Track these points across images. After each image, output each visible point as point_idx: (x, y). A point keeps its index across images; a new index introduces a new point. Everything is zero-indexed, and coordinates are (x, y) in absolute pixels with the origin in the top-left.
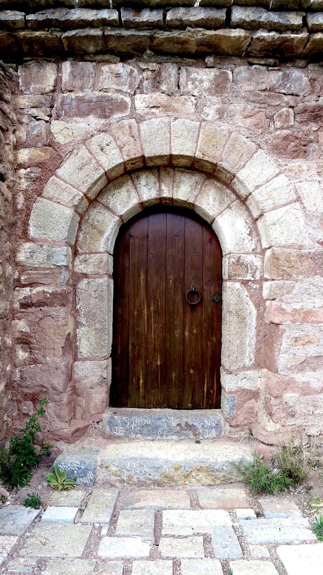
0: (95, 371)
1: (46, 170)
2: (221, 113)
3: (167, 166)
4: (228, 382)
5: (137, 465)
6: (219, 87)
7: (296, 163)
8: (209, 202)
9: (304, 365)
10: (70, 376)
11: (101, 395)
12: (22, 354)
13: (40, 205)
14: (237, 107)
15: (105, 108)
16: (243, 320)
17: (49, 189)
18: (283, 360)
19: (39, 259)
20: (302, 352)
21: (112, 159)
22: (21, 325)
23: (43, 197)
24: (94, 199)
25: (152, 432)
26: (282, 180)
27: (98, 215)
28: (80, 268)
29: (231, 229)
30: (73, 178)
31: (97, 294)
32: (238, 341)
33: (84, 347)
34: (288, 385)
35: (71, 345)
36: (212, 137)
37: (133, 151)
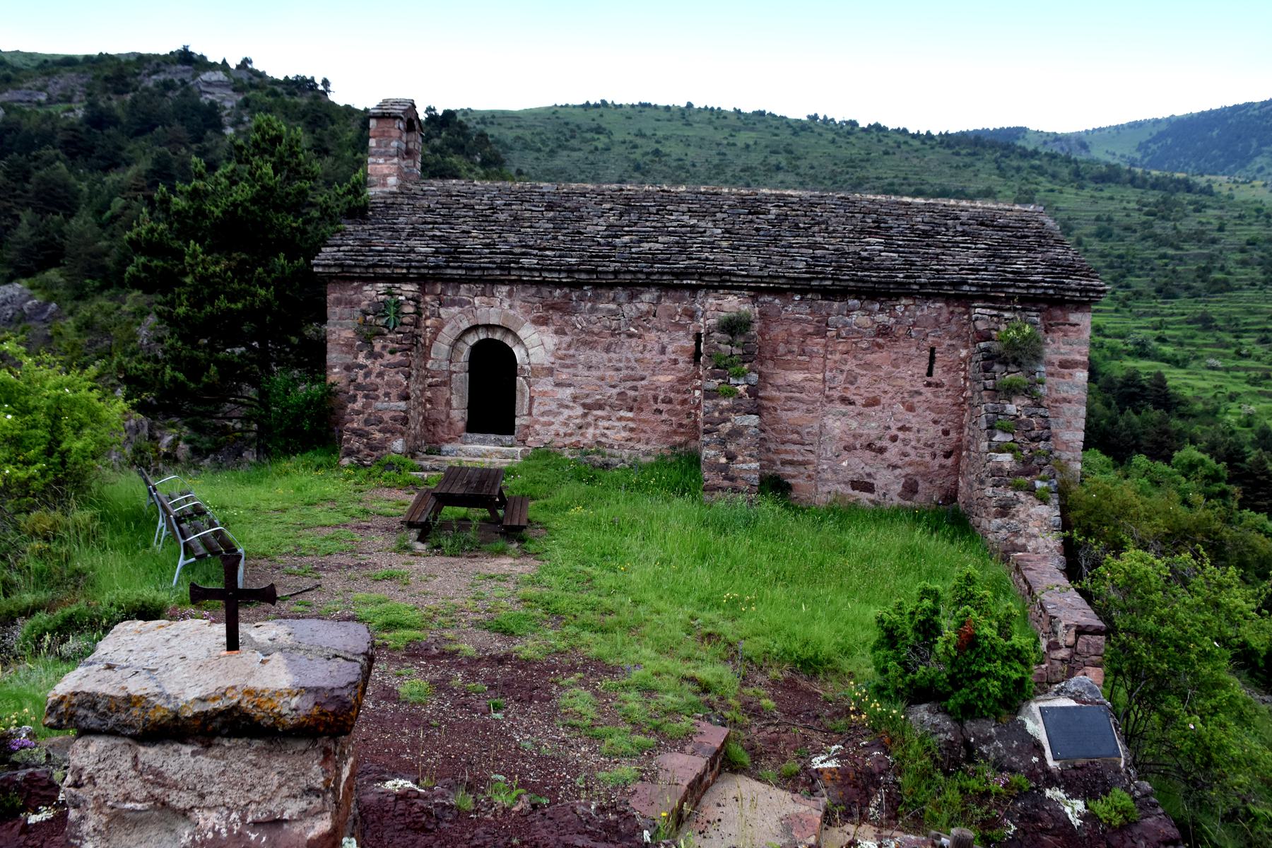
0: (459, 414)
1: (437, 330)
2: (511, 306)
3: (488, 327)
4: (518, 422)
5: (118, 203)
6: (510, 295)
7: (544, 328)
8: (509, 341)
9: (543, 414)
10: (448, 416)
11: (461, 425)
12: (428, 406)
13: (436, 344)
14: (517, 303)
15: (461, 303)
16: (523, 394)
17: (439, 338)
18: (534, 411)
19: (435, 367)
20: (542, 409)
21: (465, 325)
22: (428, 394)
23: (284, 599)
24: (453, 346)
25: (483, 442)
26: (536, 336)
27: (461, 345)
28: (453, 369)
29: (519, 352)
30: (447, 335)
31: (461, 380)
32: (521, 405)
33: (454, 404)
34: (537, 422)
35: (448, 403)
36: (507, 316)
37: (474, 322)
